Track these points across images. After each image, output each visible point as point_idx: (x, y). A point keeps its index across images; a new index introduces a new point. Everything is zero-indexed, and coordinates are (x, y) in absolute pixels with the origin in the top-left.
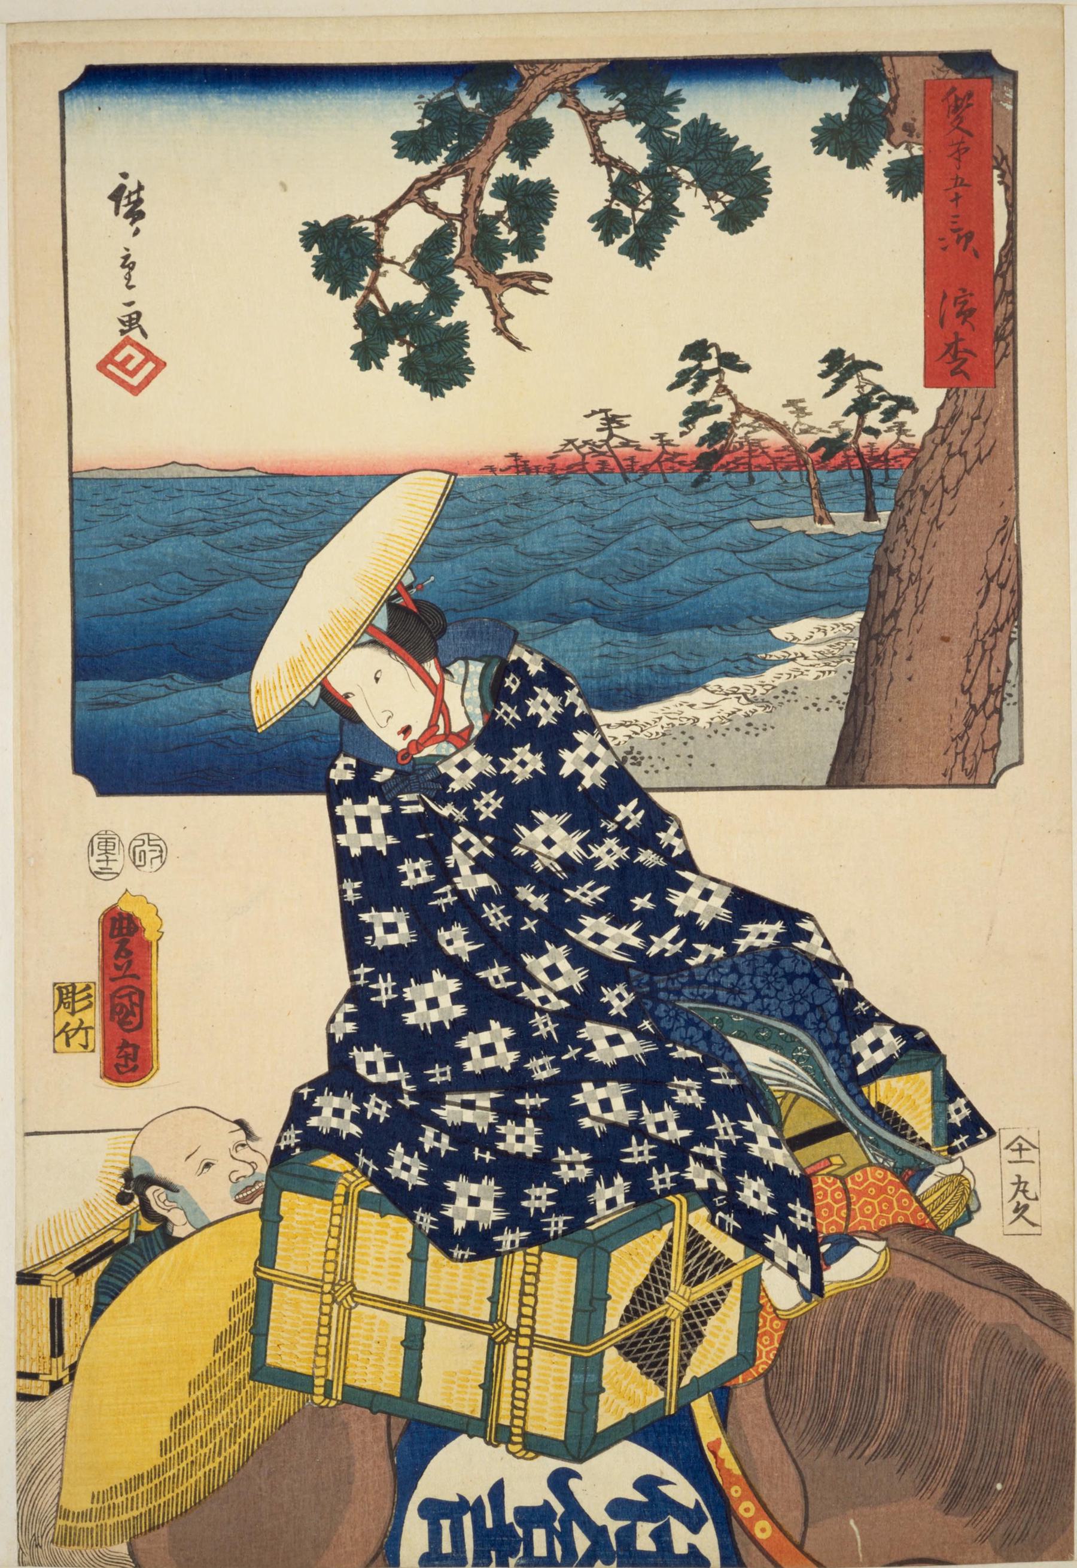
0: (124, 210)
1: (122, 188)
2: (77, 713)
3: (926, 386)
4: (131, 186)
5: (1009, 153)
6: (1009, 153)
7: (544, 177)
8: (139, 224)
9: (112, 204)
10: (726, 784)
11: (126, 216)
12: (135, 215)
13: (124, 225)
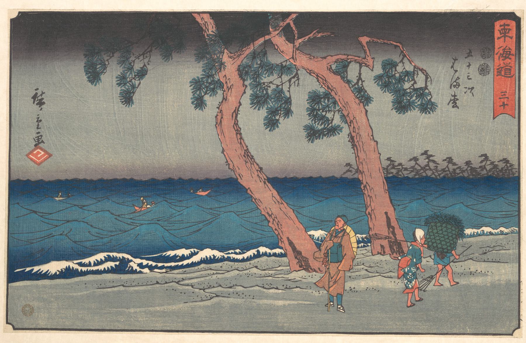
0: (36, 102)
1: (36, 94)
2: (42, 324)
3: (11, 20)
4: (39, 93)
5: (515, 163)
6: (515, 163)
7: (523, 336)
8: (43, 106)
9: (33, 100)
10: (226, 330)
11: (37, 104)
12: (41, 103)
13: (36, 107)
